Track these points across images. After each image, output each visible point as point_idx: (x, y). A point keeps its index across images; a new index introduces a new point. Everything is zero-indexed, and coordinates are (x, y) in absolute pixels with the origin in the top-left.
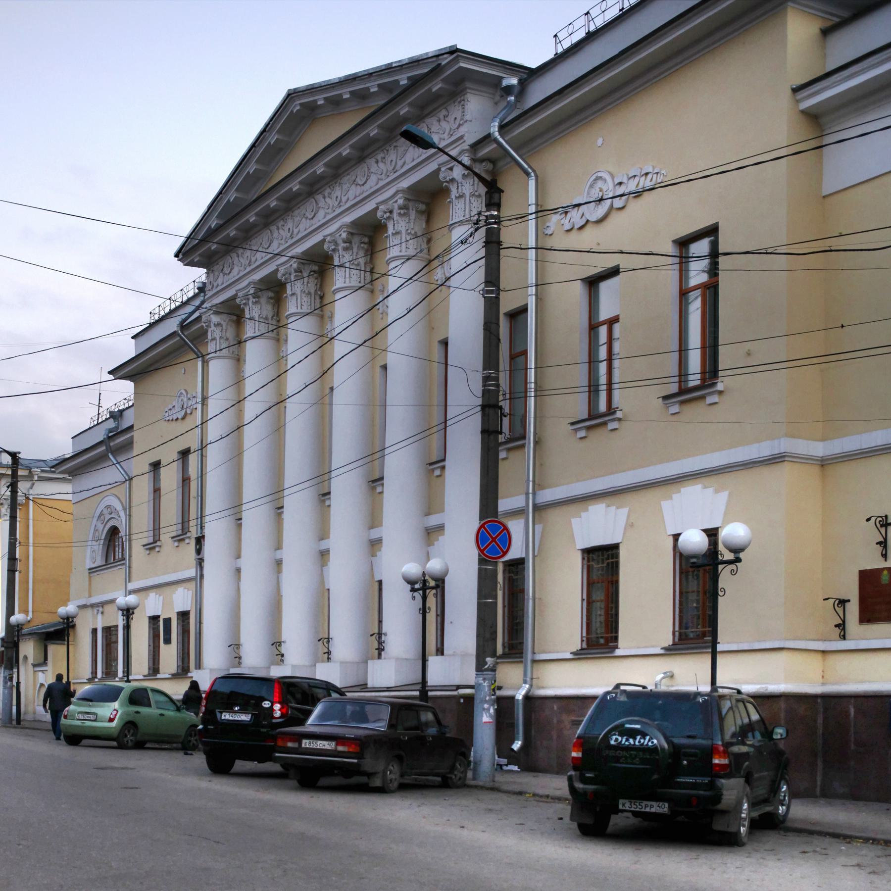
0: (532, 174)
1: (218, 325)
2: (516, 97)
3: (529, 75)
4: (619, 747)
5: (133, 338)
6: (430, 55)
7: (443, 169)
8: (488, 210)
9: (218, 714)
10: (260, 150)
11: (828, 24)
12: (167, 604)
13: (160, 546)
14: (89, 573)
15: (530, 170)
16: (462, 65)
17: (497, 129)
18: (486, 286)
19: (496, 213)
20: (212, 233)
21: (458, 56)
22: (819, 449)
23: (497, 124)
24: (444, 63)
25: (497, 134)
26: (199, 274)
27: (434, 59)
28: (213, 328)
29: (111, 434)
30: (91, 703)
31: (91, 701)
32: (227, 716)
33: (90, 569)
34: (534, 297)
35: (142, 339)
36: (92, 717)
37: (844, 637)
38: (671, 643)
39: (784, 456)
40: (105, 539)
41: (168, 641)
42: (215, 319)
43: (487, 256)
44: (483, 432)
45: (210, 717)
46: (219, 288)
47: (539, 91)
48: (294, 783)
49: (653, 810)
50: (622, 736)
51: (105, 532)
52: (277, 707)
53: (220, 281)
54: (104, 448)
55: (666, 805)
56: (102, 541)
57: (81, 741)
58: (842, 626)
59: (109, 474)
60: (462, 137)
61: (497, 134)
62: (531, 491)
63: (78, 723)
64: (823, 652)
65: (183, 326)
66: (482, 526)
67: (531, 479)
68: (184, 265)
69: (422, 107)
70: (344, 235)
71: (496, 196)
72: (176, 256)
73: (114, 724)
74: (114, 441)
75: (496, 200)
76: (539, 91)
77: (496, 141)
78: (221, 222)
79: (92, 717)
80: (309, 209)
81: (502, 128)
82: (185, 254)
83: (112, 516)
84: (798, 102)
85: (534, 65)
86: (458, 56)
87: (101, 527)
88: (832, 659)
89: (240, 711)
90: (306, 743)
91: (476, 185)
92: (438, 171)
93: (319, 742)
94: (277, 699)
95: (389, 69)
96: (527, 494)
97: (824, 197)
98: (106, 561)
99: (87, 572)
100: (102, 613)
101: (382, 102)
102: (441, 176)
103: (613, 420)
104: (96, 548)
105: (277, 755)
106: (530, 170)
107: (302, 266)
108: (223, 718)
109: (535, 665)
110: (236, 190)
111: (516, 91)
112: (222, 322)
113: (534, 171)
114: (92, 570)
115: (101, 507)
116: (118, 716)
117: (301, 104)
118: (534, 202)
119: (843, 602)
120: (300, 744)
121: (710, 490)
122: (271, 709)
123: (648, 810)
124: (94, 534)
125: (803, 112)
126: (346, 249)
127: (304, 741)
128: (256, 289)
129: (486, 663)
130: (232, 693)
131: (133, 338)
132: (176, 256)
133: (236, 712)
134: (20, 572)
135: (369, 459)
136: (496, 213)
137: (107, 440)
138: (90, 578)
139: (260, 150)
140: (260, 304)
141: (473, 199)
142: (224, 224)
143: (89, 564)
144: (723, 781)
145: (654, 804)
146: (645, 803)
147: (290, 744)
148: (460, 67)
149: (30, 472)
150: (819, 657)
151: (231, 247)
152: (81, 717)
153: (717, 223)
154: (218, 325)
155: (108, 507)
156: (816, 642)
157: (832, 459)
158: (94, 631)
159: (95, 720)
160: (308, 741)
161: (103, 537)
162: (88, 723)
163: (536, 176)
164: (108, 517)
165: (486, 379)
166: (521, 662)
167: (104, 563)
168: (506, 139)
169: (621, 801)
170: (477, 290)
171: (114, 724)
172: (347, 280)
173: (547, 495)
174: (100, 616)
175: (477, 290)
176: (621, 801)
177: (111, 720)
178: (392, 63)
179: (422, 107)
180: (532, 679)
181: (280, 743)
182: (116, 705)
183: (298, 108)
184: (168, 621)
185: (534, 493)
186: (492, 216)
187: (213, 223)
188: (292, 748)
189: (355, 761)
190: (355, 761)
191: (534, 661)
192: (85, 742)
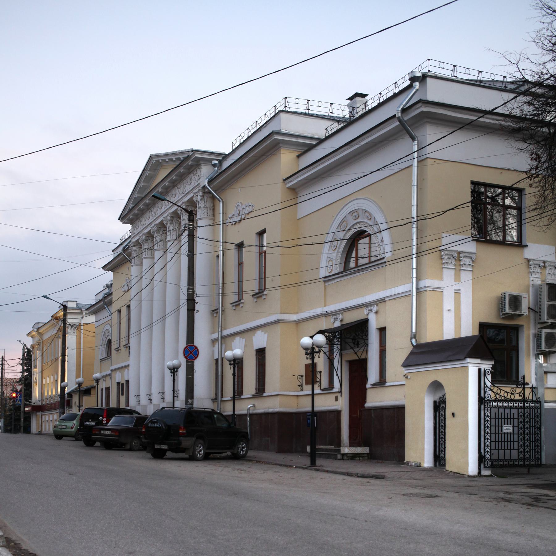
0: (221, 201)
1: (135, 251)
2: (218, 168)
3: (225, 157)
4: (151, 427)
5: (112, 251)
6: (187, 151)
7: (195, 196)
8: (189, 223)
9: (84, 422)
10: (144, 177)
11: (299, 153)
12: (122, 376)
13: (120, 350)
14: (101, 361)
15: (220, 199)
16: (196, 156)
17: (207, 183)
18: (189, 252)
19: (192, 224)
20: (131, 210)
21: (194, 153)
22: (294, 317)
23: (207, 181)
24: (190, 154)
25: (207, 185)
26: (129, 227)
27: (188, 152)
28: (133, 252)
29: (105, 296)
30: (64, 421)
31: (65, 420)
32: (87, 423)
33: (100, 360)
34: (221, 251)
35: (115, 252)
36: (65, 427)
37: (302, 390)
38: (255, 393)
39: (279, 321)
40: (107, 344)
41: (123, 394)
42: (134, 248)
43: (189, 241)
44: (187, 310)
45: (82, 423)
46: (135, 234)
47: (226, 164)
48: (149, 455)
49: (164, 448)
50: (151, 423)
51: (107, 341)
52: (105, 419)
53: (135, 231)
54: (103, 303)
55: (167, 446)
56: (106, 345)
57: (63, 437)
58: (301, 386)
59: (104, 314)
60: (199, 184)
61: (207, 185)
62: (220, 331)
63: (59, 430)
64: (297, 396)
65: (124, 250)
66: (186, 347)
67: (220, 326)
68: (123, 223)
69: (189, 169)
70: (169, 218)
71: (192, 217)
72: (119, 219)
73: (73, 430)
74: (107, 299)
75: (192, 219)
76: (226, 164)
77: (206, 187)
78: (133, 206)
79: (65, 427)
80: (160, 205)
81: (209, 182)
82: (123, 218)
83: (109, 334)
84: (286, 184)
85: (227, 153)
86: (194, 153)
87: (105, 339)
88: (300, 398)
89: (92, 421)
90: (102, 432)
91: (205, 203)
92: (193, 197)
93: (106, 431)
94: (105, 416)
95: (176, 153)
96: (219, 332)
97: (298, 219)
98: (108, 355)
99: (99, 361)
100: (105, 381)
101: (178, 163)
102: (194, 199)
103: (241, 303)
104: (103, 349)
105: (93, 436)
106: (220, 199)
107: (159, 228)
108: (86, 424)
109: (222, 403)
110: (137, 193)
111: (218, 165)
112: (137, 249)
113: (222, 199)
114: (102, 360)
115: (105, 330)
116: (75, 426)
117: (155, 160)
118: (222, 212)
119: (302, 376)
120: (100, 432)
121: (263, 333)
122: (102, 420)
123: (162, 448)
124: (102, 343)
125: (288, 188)
126: (171, 224)
127: (101, 431)
128: (146, 237)
129: (188, 402)
130: (95, 414)
131: (112, 251)
132: (119, 219)
133: (90, 422)
134: (68, 362)
135: (163, 319)
136: (192, 224)
137: (104, 299)
138: (101, 363)
139: (144, 177)
140: (148, 243)
141: (204, 209)
142: (135, 206)
143: (101, 357)
144: (182, 438)
145: (164, 446)
146: (161, 445)
147: (97, 432)
148: (195, 157)
149: (81, 311)
150: (295, 398)
151: (142, 213)
152: (60, 427)
153: (265, 229)
154: (135, 251)
155: (107, 330)
156: (295, 392)
157: (307, 319)
158: (102, 389)
159: (66, 429)
160: (102, 431)
161: (106, 343)
162: (63, 430)
163: (223, 201)
164: (107, 334)
165: (189, 289)
166: (216, 402)
167: (107, 356)
168: (211, 187)
169: (155, 445)
170: (185, 254)
171: (73, 430)
172: (171, 237)
173: (226, 332)
174: (104, 382)
175: (185, 254)
176: (155, 445)
177: (72, 428)
178: (177, 151)
179: (189, 169)
180: (221, 408)
181: (94, 432)
182: (75, 422)
183: (154, 162)
184: (123, 384)
185: (221, 332)
186: (190, 225)
187: (131, 206)
188: (97, 434)
189: (117, 438)
190: (117, 438)
191: (222, 401)
192: (64, 438)
